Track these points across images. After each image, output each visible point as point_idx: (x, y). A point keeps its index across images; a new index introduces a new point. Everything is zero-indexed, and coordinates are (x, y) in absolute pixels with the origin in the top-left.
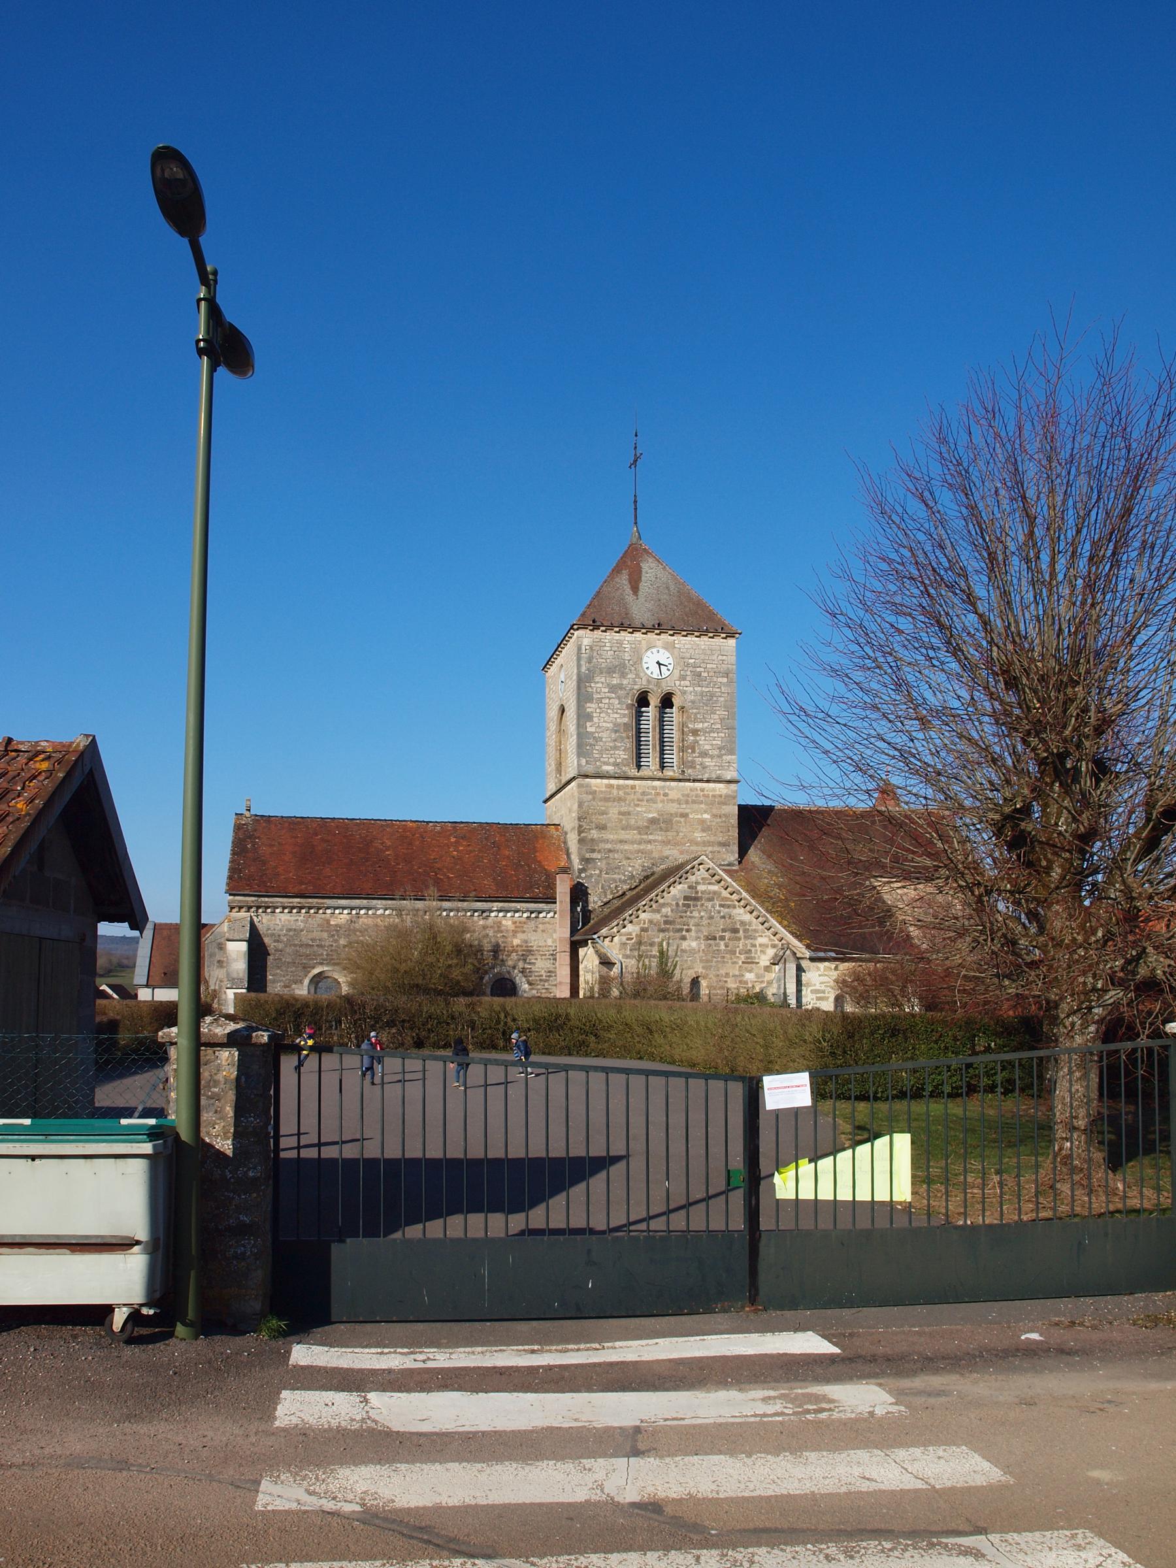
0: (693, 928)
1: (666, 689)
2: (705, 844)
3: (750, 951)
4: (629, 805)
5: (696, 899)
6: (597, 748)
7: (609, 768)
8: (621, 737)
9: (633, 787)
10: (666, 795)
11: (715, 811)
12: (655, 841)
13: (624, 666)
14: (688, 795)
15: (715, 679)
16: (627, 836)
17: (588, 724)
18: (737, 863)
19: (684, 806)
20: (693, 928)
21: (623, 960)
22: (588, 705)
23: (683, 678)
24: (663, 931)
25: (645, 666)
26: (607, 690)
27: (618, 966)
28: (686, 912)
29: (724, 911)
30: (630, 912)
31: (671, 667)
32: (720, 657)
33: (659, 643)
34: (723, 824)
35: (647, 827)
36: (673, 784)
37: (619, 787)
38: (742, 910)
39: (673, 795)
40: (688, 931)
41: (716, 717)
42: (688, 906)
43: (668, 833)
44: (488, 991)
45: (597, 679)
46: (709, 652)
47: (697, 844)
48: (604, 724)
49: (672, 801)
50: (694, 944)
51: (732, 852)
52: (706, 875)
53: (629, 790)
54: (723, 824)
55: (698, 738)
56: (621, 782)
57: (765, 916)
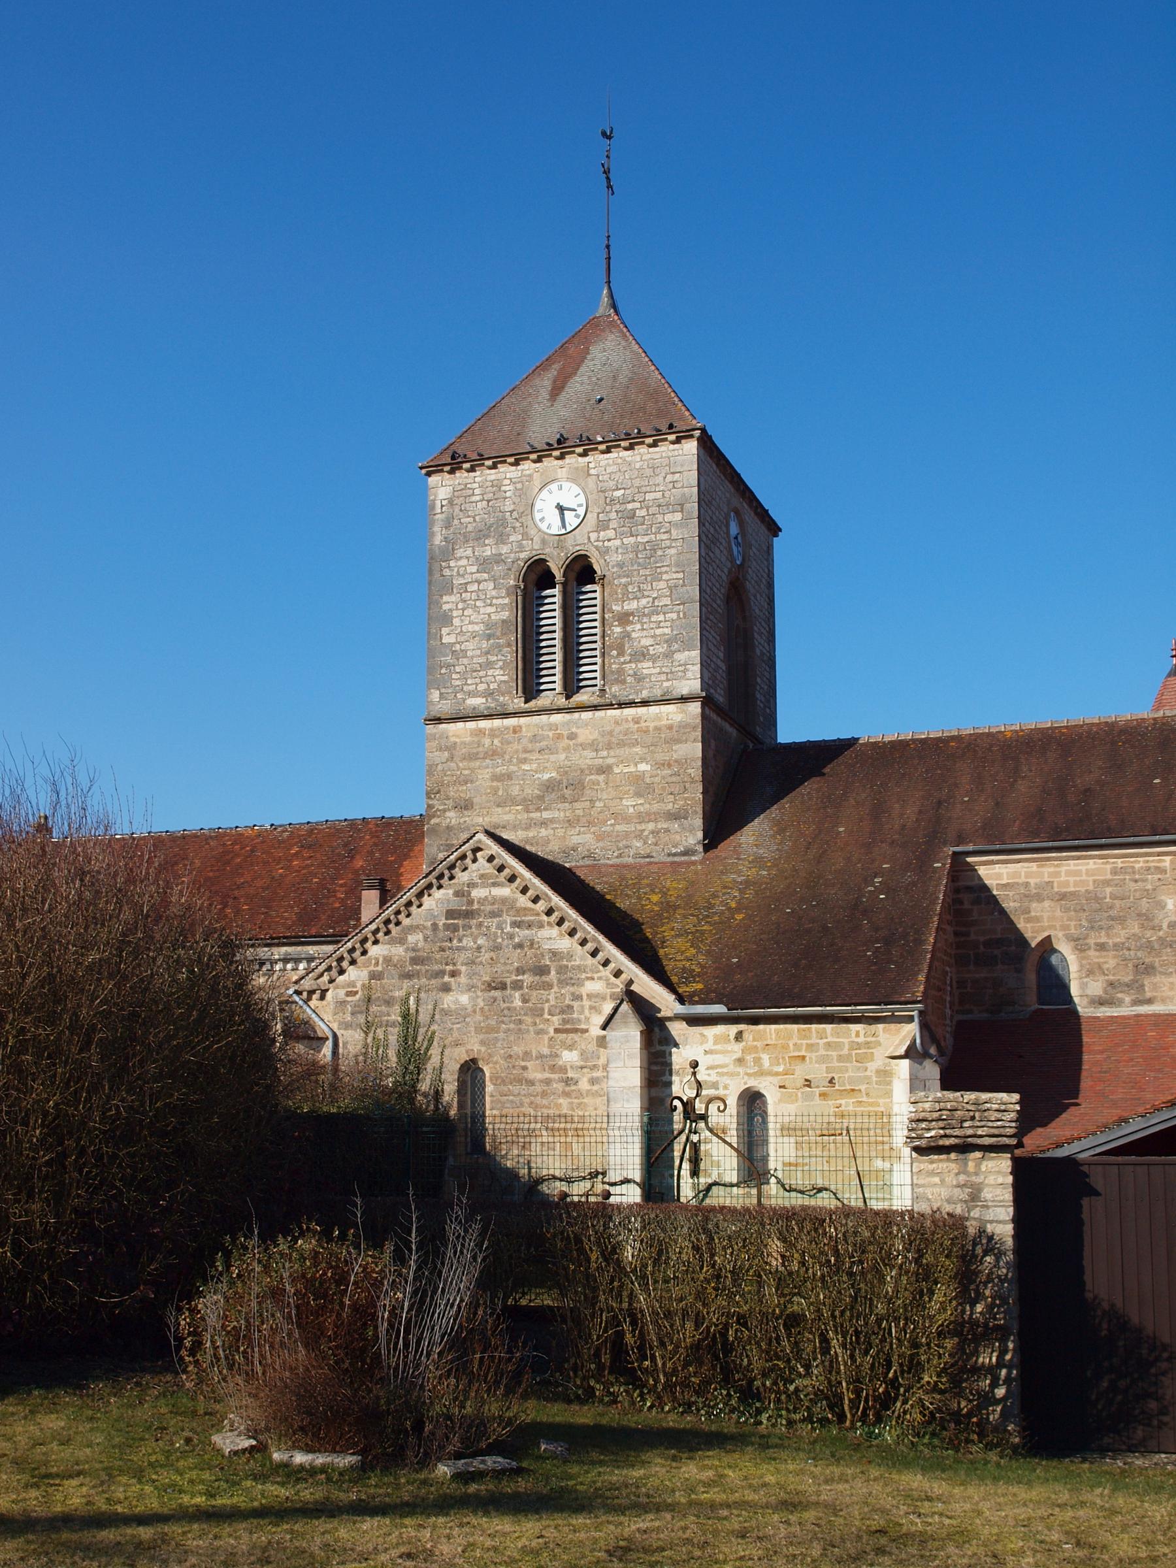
0: (463, 969)
1: (573, 546)
2: (642, 818)
3: (570, 1007)
4: (510, 761)
5: (469, 914)
6: (458, 669)
7: (477, 702)
8: (499, 646)
9: (516, 730)
10: (572, 737)
11: (660, 757)
12: (552, 821)
13: (503, 522)
14: (611, 733)
15: (660, 518)
16: (506, 817)
17: (445, 631)
18: (700, 848)
19: (605, 753)
20: (463, 969)
21: (339, 1033)
22: (445, 598)
23: (602, 526)
24: (408, 976)
25: (538, 516)
26: (474, 569)
27: (329, 1043)
28: (451, 940)
29: (522, 934)
30: (349, 945)
31: (581, 511)
32: (670, 478)
33: (562, 473)
34: (674, 779)
35: (541, 798)
36: (586, 715)
37: (493, 733)
38: (555, 931)
39: (585, 735)
40: (453, 974)
41: (662, 585)
42: (455, 929)
43: (577, 805)
44: (654, 1094)
45: (459, 553)
46: (649, 472)
47: (627, 819)
48: (470, 628)
49: (583, 746)
50: (464, 999)
51: (692, 830)
52: (489, 869)
53: (510, 736)
54: (674, 779)
55: (629, 628)
56: (497, 723)
57: (595, 939)
